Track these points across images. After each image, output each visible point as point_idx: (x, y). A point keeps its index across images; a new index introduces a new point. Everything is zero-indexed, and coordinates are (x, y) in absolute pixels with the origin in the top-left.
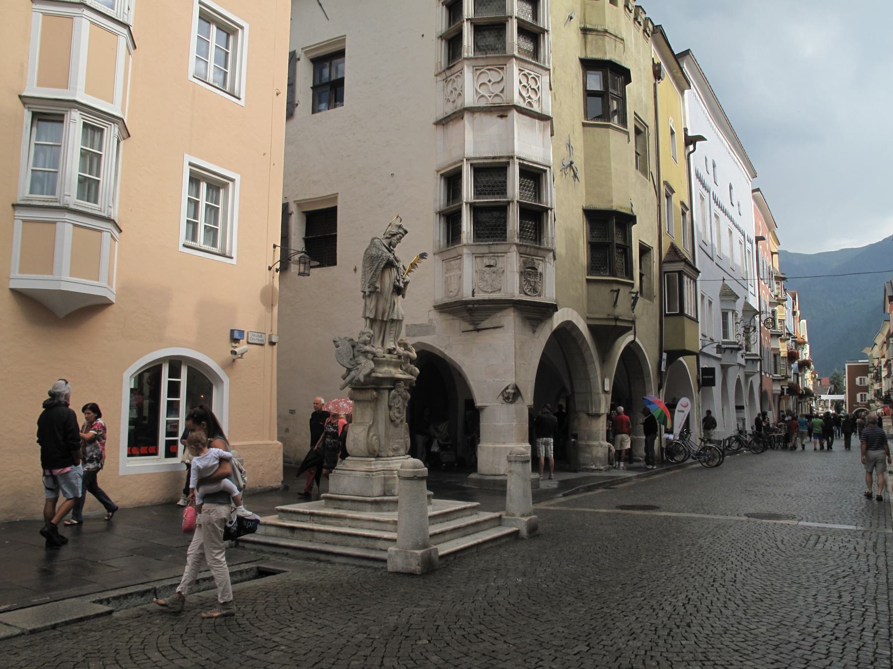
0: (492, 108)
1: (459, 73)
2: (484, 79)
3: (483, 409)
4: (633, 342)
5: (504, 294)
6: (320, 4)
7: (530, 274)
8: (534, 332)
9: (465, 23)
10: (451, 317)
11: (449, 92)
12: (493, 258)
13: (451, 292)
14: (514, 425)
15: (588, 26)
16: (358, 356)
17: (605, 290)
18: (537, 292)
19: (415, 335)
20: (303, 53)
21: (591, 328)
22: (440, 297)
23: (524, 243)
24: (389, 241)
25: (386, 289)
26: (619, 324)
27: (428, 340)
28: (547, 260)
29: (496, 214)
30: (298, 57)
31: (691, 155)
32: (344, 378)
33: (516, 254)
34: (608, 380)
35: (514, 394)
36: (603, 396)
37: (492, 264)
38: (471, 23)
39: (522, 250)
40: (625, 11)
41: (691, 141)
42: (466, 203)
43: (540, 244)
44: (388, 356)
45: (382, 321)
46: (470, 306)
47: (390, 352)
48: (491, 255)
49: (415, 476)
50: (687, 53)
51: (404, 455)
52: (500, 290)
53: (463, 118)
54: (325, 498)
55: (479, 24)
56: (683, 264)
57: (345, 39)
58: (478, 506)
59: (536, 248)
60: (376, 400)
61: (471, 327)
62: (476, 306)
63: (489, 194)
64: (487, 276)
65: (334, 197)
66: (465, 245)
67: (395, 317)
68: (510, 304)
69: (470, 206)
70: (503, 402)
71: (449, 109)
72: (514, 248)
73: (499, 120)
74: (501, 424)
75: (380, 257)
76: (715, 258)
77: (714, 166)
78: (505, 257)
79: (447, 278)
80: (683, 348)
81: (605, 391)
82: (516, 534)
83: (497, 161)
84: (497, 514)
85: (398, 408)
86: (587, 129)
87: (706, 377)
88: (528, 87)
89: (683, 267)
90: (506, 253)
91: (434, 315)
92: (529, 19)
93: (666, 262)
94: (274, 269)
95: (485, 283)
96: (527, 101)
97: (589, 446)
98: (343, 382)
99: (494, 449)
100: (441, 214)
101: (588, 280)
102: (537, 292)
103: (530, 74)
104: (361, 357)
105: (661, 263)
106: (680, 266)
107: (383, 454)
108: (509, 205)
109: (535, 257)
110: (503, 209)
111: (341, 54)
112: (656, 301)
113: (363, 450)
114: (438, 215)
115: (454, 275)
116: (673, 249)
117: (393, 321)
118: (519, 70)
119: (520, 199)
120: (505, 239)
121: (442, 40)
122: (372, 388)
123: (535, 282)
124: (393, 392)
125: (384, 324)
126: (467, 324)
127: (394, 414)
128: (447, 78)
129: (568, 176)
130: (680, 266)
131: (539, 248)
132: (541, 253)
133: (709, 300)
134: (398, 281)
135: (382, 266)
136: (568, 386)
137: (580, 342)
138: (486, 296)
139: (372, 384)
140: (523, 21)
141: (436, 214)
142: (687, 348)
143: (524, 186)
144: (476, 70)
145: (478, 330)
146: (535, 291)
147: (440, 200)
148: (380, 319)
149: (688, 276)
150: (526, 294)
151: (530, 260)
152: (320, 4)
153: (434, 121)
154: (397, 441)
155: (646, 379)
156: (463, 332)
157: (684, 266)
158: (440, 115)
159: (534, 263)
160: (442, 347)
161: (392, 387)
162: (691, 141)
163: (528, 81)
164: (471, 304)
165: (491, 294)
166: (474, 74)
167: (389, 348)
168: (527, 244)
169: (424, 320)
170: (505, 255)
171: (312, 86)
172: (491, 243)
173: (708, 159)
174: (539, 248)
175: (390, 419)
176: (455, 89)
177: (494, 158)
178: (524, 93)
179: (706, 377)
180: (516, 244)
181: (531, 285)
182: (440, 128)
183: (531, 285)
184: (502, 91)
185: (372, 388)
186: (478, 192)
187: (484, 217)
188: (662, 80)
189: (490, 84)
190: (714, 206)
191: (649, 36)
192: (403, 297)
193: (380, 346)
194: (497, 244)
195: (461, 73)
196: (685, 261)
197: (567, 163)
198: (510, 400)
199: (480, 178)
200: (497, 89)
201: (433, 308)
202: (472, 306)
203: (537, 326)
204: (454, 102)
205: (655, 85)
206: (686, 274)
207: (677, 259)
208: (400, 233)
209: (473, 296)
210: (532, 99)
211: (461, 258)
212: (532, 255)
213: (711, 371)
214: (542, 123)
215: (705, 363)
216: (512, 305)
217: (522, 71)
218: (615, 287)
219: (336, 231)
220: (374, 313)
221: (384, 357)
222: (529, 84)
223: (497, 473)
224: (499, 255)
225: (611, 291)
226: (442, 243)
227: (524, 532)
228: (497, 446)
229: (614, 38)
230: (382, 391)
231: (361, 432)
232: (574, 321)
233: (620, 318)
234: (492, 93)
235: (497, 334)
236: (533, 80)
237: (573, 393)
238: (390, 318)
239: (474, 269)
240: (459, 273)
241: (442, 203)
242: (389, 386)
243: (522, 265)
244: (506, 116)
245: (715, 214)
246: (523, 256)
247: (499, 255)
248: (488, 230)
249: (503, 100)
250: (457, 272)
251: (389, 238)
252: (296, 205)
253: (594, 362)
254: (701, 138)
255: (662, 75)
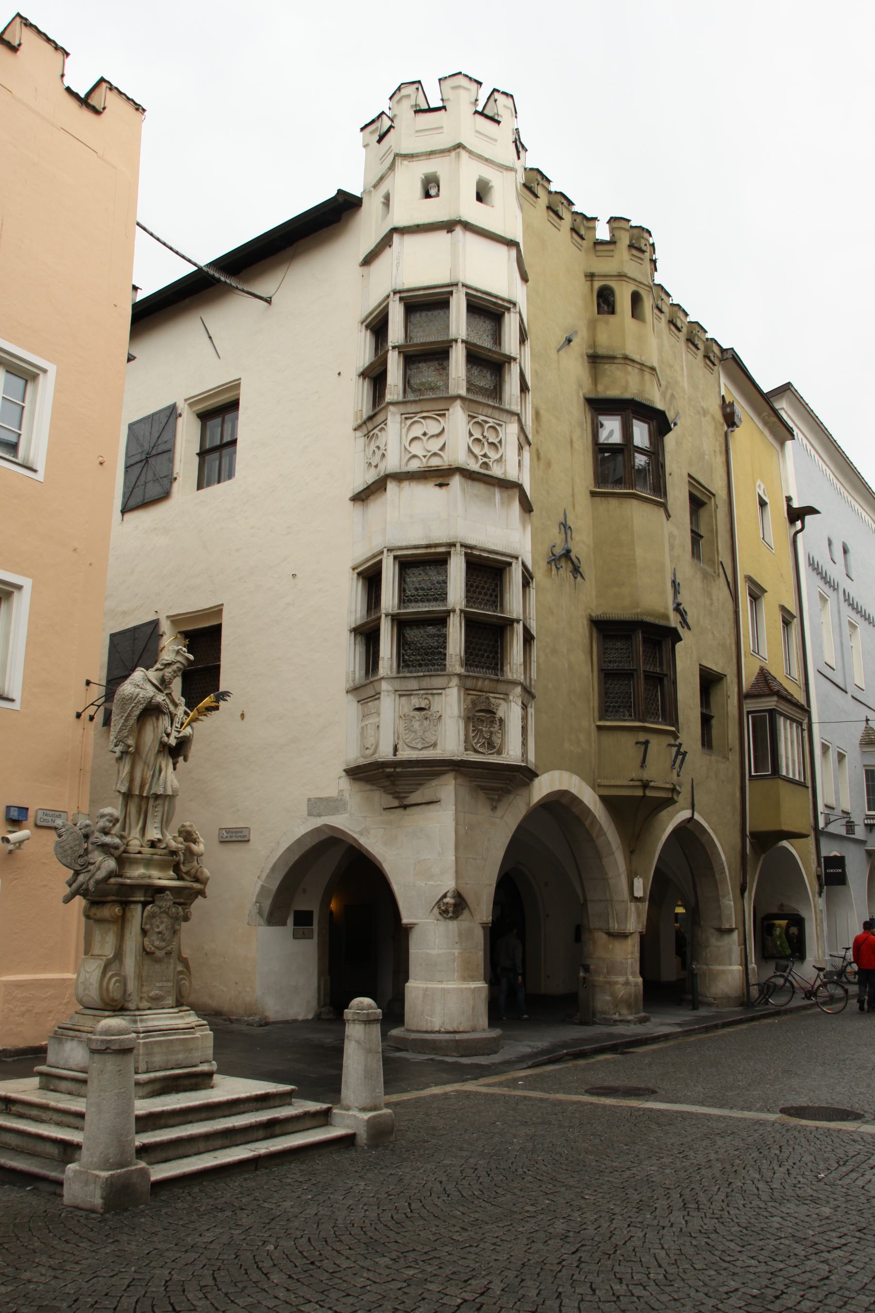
0: (427, 473)
1: (382, 426)
2: (417, 431)
3: (412, 928)
4: (691, 819)
5: (440, 752)
6: (210, 337)
7: (482, 721)
8: (494, 808)
9: (390, 353)
10: (369, 787)
11: (371, 452)
12: (425, 696)
13: (367, 748)
14: (456, 954)
15: (601, 351)
16: (93, 851)
17: (628, 742)
18: (494, 747)
19: (320, 815)
20: (186, 406)
21: (605, 800)
22: (354, 756)
23: (471, 674)
24: (160, 673)
25: (147, 748)
26: (649, 793)
27: (339, 821)
28: (511, 698)
29: (431, 630)
30: (179, 411)
31: (800, 535)
32: (70, 886)
33: (459, 691)
34: (641, 880)
35: (455, 905)
36: (632, 906)
37: (423, 706)
38: (399, 352)
39: (469, 683)
40: (670, 329)
41: (797, 515)
42: (387, 615)
43: (502, 675)
44: (147, 850)
45: (141, 796)
46: (388, 770)
47: (153, 844)
48: (422, 692)
49: (107, 1048)
50: (786, 389)
51: (172, 1007)
52: (434, 745)
53: (385, 489)
54: (41, 1074)
55: (410, 353)
56: (775, 698)
57: (239, 384)
58: (293, 1091)
59: (491, 680)
60: (122, 921)
61: (396, 803)
62: (398, 770)
63: (422, 601)
64: (416, 725)
65: (217, 611)
66: (382, 678)
67: (160, 791)
68: (449, 766)
69: (393, 620)
70: (440, 917)
71: (371, 477)
72: (455, 681)
73: (437, 489)
74: (435, 952)
75: (136, 697)
76: (851, 690)
77: (845, 551)
78: (443, 695)
79: (362, 728)
80: (777, 828)
81: (636, 898)
82: (348, 1141)
83: (433, 550)
84: (325, 1106)
85: (159, 933)
86: (598, 499)
87: (832, 871)
88: (484, 440)
89: (774, 703)
90: (444, 689)
91: (345, 784)
92: (486, 342)
93: (748, 696)
94: (85, 716)
95: (413, 734)
96: (481, 462)
97: (609, 983)
98: (67, 890)
99: (426, 989)
100: (357, 631)
101: (599, 728)
102: (494, 747)
103: (486, 422)
104: (96, 853)
105: (743, 697)
106: (770, 703)
107: (132, 1006)
108: (449, 616)
109: (491, 695)
110: (441, 620)
111: (233, 406)
112: (735, 757)
113: (95, 998)
114: (353, 633)
115: (371, 724)
116: (764, 676)
117: (157, 797)
118: (469, 416)
119: (467, 607)
120: (443, 667)
121: (364, 378)
122: (113, 901)
123: (491, 733)
124: (149, 907)
125: (144, 801)
126: (390, 797)
127: (152, 943)
128: (369, 432)
129: (561, 571)
130: (770, 703)
131: (498, 681)
132: (502, 688)
133: (838, 752)
134: (168, 735)
135: (137, 713)
136: (579, 891)
137: (587, 823)
138: (414, 755)
139: (113, 895)
140: (475, 345)
141: (351, 632)
142: (785, 828)
143: (477, 587)
144: (406, 418)
145: (405, 807)
146: (491, 745)
147: (356, 611)
148: (137, 793)
149: (787, 717)
150: (476, 751)
151: (482, 699)
152: (210, 337)
153: (350, 495)
154: (158, 984)
155: (717, 877)
156: (385, 809)
157: (777, 701)
158: (359, 486)
159: (489, 703)
160: (356, 832)
161: (150, 899)
162: (797, 515)
163: (483, 432)
164: (391, 767)
165: (422, 752)
166: (403, 425)
167: (152, 838)
168: (476, 675)
169: (331, 792)
170: (443, 691)
171: (198, 451)
172: (421, 674)
173: (834, 541)
174: (498, 681)
175: (144, 949)
176: (378, 448)
177: (428, 546)
178: (477, 450)
179: (832, 871)
180: (459, 675)
181: (484, 738)
182: (359, 504)
183: (484, 738)
184: (442, 448)
185: (113, 901)
186: (404, 598)
187: (413, 634)
188: (738, 427)
189: (425, 439)
190: (847, 611)
191: (714, 364)
192: (185, 760)
193: (138, 836)
194: (430, 676)
195: (386, 424)
196: (785, 698)
197: (558, 551)
198: (450, 915)
199: (410, 578)
200: (434, 445)
201: (344, 774)
202: (392, 770)
203: (499, 800)
204: (376, 466)
205: (726, 435)
206: (781, 714)
207: (767, 692)
208: (179, 662)
209: (395, 755)
210: (489, 458)
211: (379, 698)
212: (486, 692)
213: (838, 862)
214: (506, 494)
215: (830, 850)
216: (451, 768)
217: (474, 417)
218: (642, 737)
219: (220, 661)
220: (127, 785)
221: (140, 853)
222: (484, 437)
223: (429, 1029)
224: (435, 691)
225: (637, 743)
226: (357, 676)
227: (363, 1136)
228: (430, 986)
229: (638, 366)
230: (132, 906)
231: (94, 971)
232: (574, 791)
233: (652, 784)
234: (429, 452)
235: (432, 812)
236: (491, 430)
237: (585, 900)
238: (152, 792)
239: (397, 714)
240: (377, 720)
241: (359, 615)
242: (142, 899)
243: (470, 706)
244: (448, 484)
245: (850, 623)
246: (472, 692)
247: (435, 691)
248: (419, 655)
249: (444, 462)
250: (372, 720)
251: (161, 670)
252: (169, 622)
253: (613, 853)
254: (812, 511)
255: (736, 420)
